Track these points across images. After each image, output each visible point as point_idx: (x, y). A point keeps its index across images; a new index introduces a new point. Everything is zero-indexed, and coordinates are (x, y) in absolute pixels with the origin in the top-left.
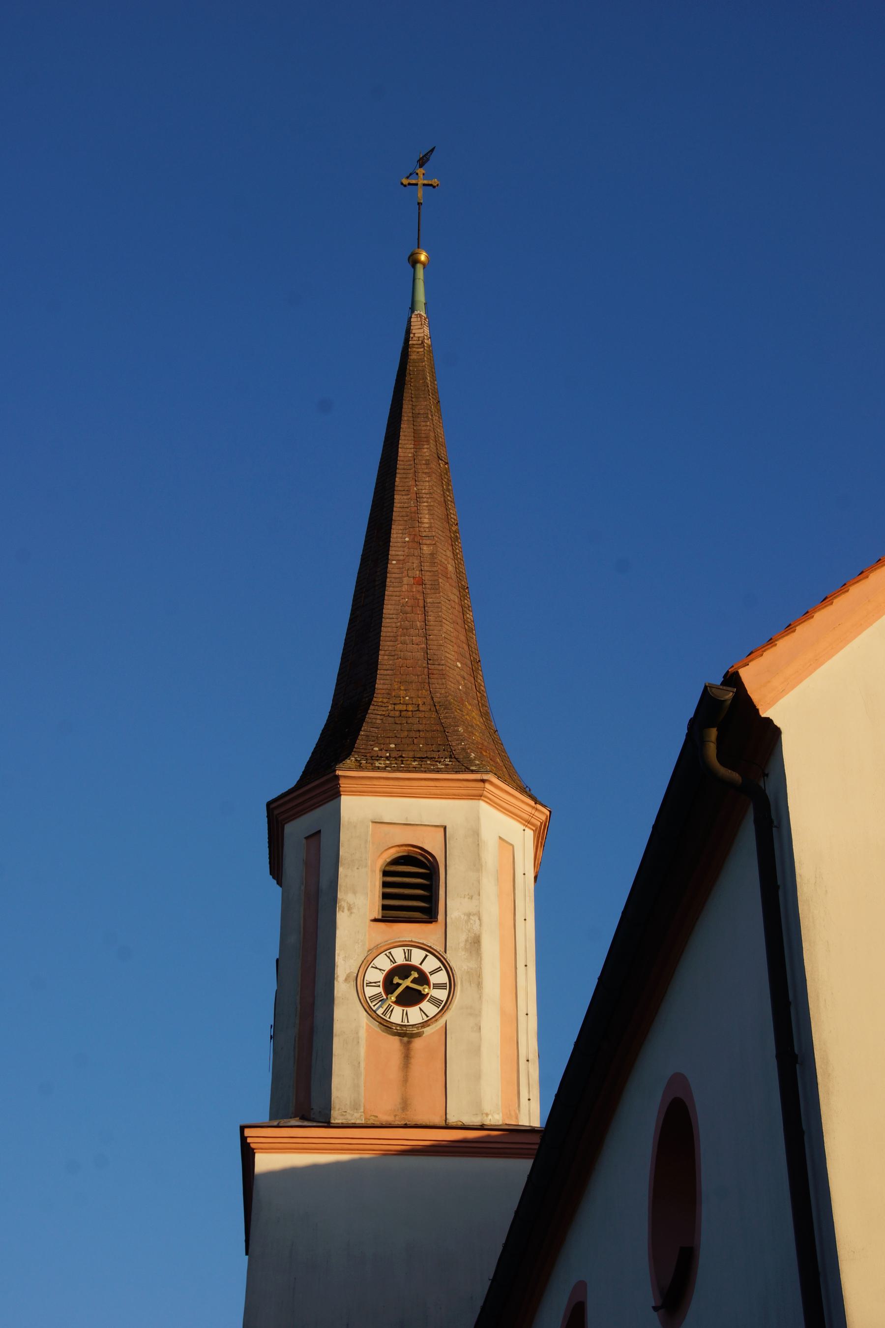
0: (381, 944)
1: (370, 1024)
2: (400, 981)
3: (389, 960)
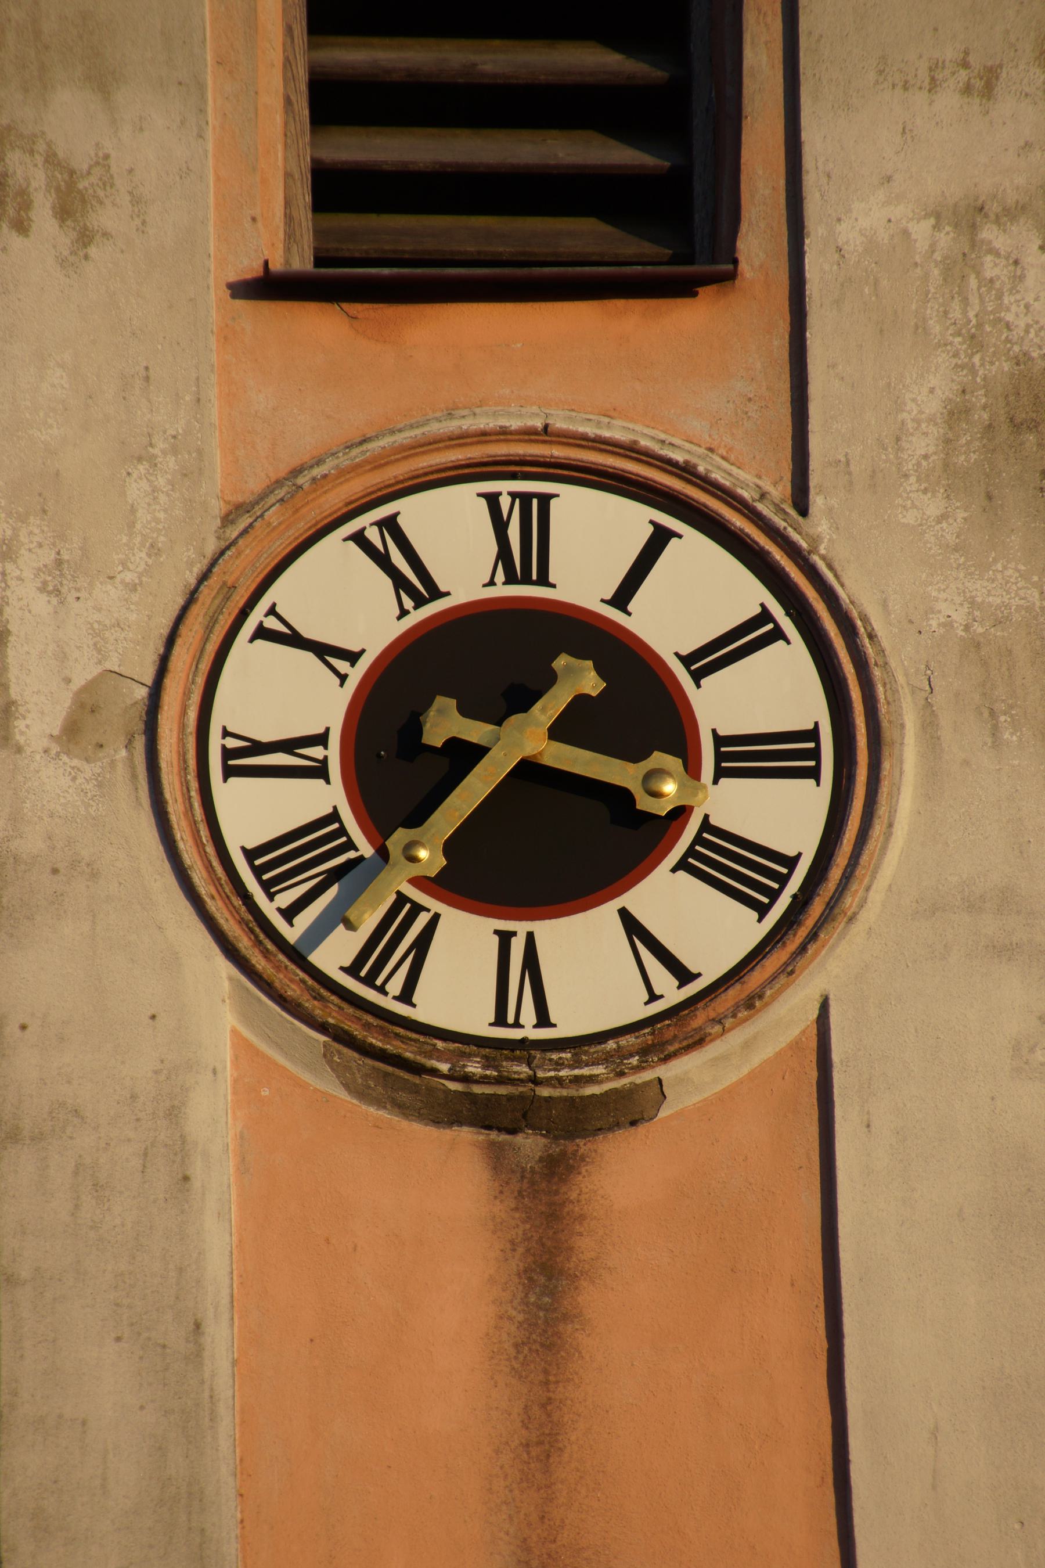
0: (319, 462)
1: (246, 1033)
2: (475, 732)
3: (265, 737)
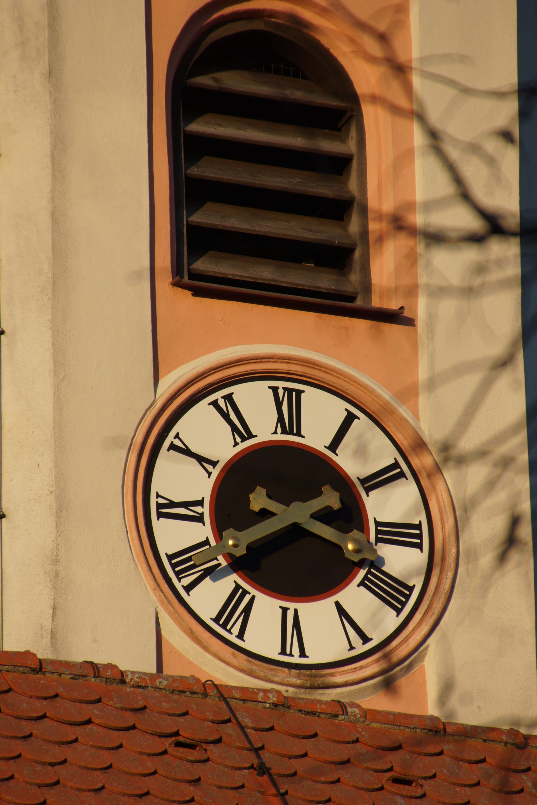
2: (273, 506)
